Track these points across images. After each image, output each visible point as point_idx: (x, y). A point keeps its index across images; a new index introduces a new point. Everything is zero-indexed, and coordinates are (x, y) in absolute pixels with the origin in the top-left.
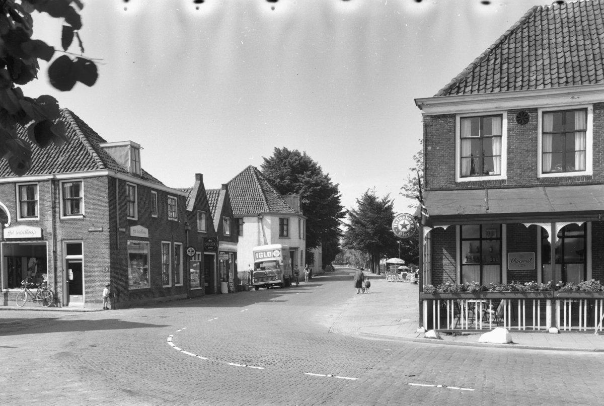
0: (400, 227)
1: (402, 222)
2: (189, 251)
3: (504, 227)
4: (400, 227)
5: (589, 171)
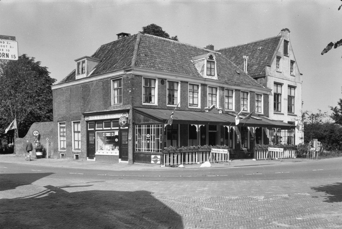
0: (123, 122)
1: (123, 120)
2: (35, 133)
3: (179, 125)
4: (123, 122)
5: (156, 104)
